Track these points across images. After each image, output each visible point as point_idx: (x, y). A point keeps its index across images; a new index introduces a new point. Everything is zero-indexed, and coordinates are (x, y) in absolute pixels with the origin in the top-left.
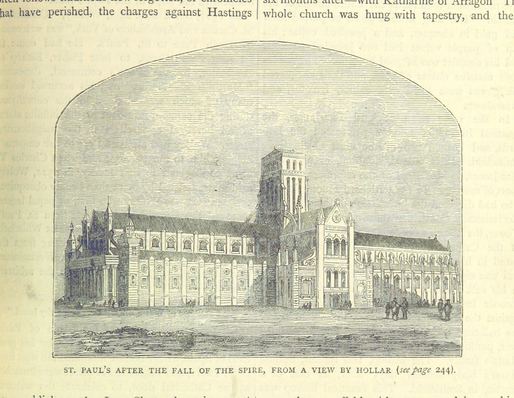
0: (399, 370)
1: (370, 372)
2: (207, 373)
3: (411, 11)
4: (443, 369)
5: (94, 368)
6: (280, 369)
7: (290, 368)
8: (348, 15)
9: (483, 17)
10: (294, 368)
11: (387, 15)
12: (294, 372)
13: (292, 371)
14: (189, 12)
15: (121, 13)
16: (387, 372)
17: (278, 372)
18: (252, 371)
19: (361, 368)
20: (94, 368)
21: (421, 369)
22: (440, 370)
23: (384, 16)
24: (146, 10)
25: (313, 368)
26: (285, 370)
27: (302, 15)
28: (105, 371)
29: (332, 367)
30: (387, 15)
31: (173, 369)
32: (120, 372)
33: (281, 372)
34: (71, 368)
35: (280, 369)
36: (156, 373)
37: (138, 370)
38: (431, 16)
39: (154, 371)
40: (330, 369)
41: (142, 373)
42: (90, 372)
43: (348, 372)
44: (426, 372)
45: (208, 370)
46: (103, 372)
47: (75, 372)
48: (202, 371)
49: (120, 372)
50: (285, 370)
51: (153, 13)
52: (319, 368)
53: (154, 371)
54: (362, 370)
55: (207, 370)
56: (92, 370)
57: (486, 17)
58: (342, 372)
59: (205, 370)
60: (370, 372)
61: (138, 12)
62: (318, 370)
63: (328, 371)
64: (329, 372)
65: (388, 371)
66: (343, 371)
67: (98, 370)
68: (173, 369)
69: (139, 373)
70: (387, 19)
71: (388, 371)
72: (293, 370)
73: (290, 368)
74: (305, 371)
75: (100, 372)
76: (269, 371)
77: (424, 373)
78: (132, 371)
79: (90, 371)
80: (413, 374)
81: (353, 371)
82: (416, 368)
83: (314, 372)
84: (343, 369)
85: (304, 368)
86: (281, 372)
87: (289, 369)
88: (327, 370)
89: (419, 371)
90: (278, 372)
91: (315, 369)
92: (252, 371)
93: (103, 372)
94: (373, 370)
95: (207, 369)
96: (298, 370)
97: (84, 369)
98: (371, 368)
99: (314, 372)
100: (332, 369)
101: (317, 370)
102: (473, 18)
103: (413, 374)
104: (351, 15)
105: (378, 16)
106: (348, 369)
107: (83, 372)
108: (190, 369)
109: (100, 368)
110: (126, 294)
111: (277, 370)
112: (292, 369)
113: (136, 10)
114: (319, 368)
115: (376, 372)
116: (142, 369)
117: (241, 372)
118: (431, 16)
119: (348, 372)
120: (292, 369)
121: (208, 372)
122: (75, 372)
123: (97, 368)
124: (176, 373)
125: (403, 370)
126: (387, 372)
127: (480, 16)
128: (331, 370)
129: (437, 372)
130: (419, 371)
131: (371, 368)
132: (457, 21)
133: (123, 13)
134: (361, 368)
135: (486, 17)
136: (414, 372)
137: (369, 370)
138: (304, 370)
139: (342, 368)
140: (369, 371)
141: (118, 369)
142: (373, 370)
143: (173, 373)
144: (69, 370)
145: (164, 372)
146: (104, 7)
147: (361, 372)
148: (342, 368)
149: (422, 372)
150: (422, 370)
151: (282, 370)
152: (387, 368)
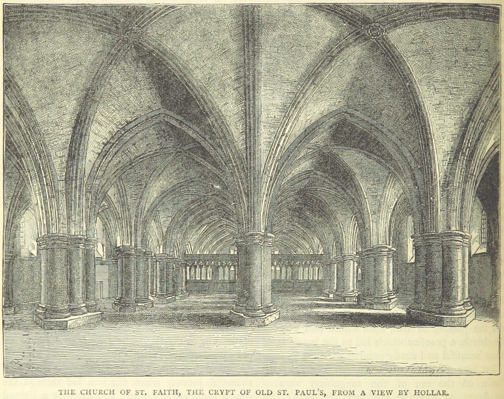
5: (307, 391)
6: (340, 392)
12: (354, 394)
13: (351, 394)
18: (380, 393)
20: (307, 391)
25: (372, 391)
28: (319, 393)
29: (391, 390)
31: (154, 391)
32: (440, 395)
33: (102, 394)
34: (284, 391)
35: (340, 392)
39: (191, 393)
40: (388, 392)
42: (304, 395)
45: (128, 391)
46: (316, 395)
47: (146, 394)
48: (258, 393)
49: (440, 395)
50: (345, 393)
52: (378, 391)
53: (191, 393)
55: (127, 392)
58: (400, 395)
59: (126, 392)
62: (377, 392)
63: (386, 394)
64: (388, 394)
66: (401, 394)
67: (312, 392)
68: (154, 391)
74: (364, 393)
83: (374, 394)
84: (401, 391)
85: (363, 391)
86: (102, 394)
88: (385, 393)
90: (339, 395)
91: (374, 392)
93: (316, 395)
94: (430, 392)
95: (127, 390)
96: (358, 392)
98: (263, 391)
99: (374, 394)
100: (391, 391)
101: (376, 393)
108: (189, 394)
109: (314, 391)
110: (164, 105)
111: (337, 393)
114: (378, 391)
115: (432, 395)
116: (445, 392)
119: (406, 395)
121: (248, 393)
122: (288, 394)
123: (310, 390)
124: (156, 394)
131: (428, 391)
137: (426, 392)
139: (400, 391)
140: (426, 393)
141: (439, 391)
143: (154, 394)
145: (201, 393)
148: (400, 391)
151: (342, 393)
152: (443, 391)
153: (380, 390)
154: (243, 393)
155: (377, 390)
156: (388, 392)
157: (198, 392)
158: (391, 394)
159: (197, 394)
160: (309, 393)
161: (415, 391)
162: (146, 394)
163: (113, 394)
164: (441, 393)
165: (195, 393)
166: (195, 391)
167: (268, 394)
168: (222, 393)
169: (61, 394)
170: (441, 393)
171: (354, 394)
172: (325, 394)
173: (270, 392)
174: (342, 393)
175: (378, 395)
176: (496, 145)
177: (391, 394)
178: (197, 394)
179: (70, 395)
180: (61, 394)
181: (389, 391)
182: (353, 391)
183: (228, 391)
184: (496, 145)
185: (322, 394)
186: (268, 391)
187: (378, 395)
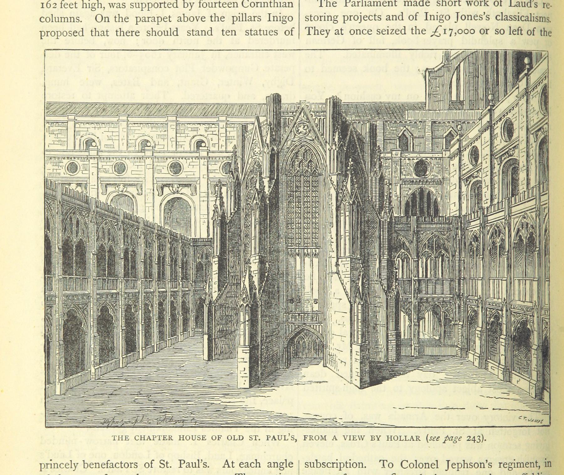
0: (429, 438)
1: (285, 440)
2: (218, 440)
3: (119, 15)
4: (474, 437)
5: (278, 436)
6: (418, 437)
7: (321, 436)
8: (150, 19)
9: (397, 19)
10: (325, 436)
11: (284, 18)
14: (72, 19)
15: (40, 19)
16: (417, 440)
17: (310, 440)
18: (352, 438)
19: (391, 436)
20: (278, 436)
21: (452, 437)
22: (471, 438)
23: (333, 19)
24: (286, 17)
26: (317, 438)
27: (498, 18)
28: (290, 438)
30: (335, 17)
31: (305, 436)
36: (119, 440)
37: (167, 438)
38: (156, 19)
39: (117, 438)
41: (419, 440)
43: (378, 440)
44: (457, 440)
48: (230, 438)
50: (317, 438)
51: (478, 18)
52: (350, 436)
54: (392, 437)
56: (276, 438)
57: (400, 18)
58: (372, 440)
60: (400, 440)
61: (147, 19)
65: (418, 438)
66: (373, 439)
67: (283, 437)
69: (169, 440)
70: (335, 22)
71: (418, 438)
72: (324, 438)
73: (321, 436)
75: (285, 440)
76: (300, 439)
77: (455, 442)
78: (162, 438)
79: (274, 438)
80: (444, 443)
81: (368, 438)
82: (447, 436)
84: (373, 437)
87: (320, 437)
88: (357, 438)
89: (450, 439)
90: (310, 440)
91: (345, 437)
92: (352, 438)
97: (269, 437)
98: (400, 436)
102: (388, 19)
103: (444, 443)
104: (507, 18)
105: (60, 20)
106: (378, 437)
107: (268, 440)
108: (406, 436)
109: (285, 436)
111: (308, 438)
112: (323, 437)
113: (389, 16)
114: (350, 436)
115: (406, 440)
117: (251, 439)
118: (156, 19)
119: (378, 440)
120: (323, 437)
124: (270, 439)
125: (432, 438)
126: (417, 440)
127: (394, 17)
128: (362, 438)
129: (468, 440)
130: (450, 439)
132: (326, 37)
133: (42, 21)
134: (391, 436)
135: (400, 18)
136: (445, 440)
138: (335, 438)
141: (412, 437)
142: (403, 438)
143: (305, 440)
144: (254, 438)
146: (215, 14)
147: (391, 440)
149: (453, 440)
150: (454, 438)
151: (313, 438)
153: (352, 435)
154: (214, 438)
155: (349, 435)
156: (360, 437)
157: (124, 438)
158: (362, 439)
159: (122, 440)
160: (280, 438)
161: (388, 436)
162: (171, 467)
163: (388, 436)
164: (415, 439)
165: (120, 439)
166: (120, 437)
167: (239, 440)
168: (378, 439)
169: (114, 440)
170: (415, 439)
171: (325, 440)
172: (296, 440)
173: (241, 438)
174: (313, 438)
175: (350, 440)
176: (546, 76)
177: (362, 439)
178: (122, 440)
179: (124, 441)
180: (114, 440)
181: (361, 436)
182: (325, 436)
183: (155, 437)
184: (546, 76)
185: (293, 439)
186: (239, 436)
187: (350, 440)
